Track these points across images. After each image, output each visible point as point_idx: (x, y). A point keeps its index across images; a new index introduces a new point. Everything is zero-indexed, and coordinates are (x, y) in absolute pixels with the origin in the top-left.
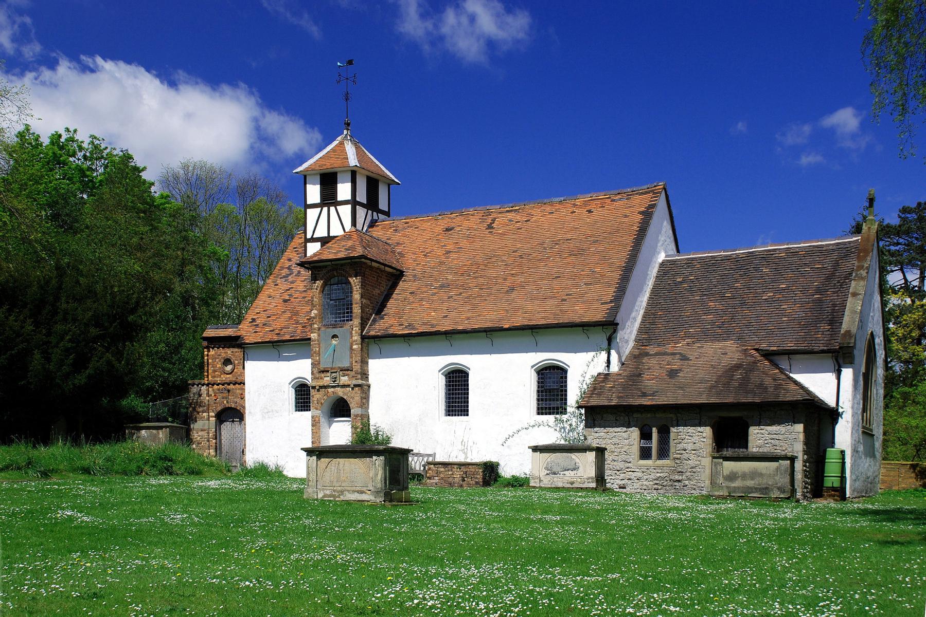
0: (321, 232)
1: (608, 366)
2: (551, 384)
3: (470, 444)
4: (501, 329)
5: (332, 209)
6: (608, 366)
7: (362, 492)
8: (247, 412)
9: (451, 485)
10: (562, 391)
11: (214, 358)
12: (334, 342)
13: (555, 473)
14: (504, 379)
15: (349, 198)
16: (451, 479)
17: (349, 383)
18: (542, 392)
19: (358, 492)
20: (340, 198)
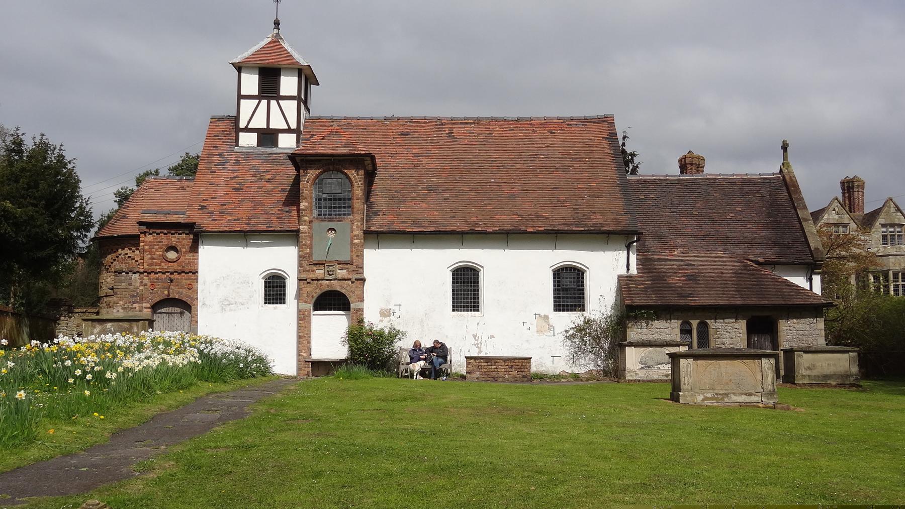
0: (259, 122)
1: (628, 269)
2: (566, 282)
3: (485, 338)
4: (525, 232)
5: (273, 103)
6: (628, 269)
7: (750, 395)
8: (200, 304)
9: (495, 379)
10: (579, 290)
11: (151, 244)
12: (331, 235)
13: (649, 367)
14: (518, 276)
15: (296, 94)
16: (494, 374)
17: (350, 277)
18: (559, 290)
19: (746, 394)
20: (283, 92)
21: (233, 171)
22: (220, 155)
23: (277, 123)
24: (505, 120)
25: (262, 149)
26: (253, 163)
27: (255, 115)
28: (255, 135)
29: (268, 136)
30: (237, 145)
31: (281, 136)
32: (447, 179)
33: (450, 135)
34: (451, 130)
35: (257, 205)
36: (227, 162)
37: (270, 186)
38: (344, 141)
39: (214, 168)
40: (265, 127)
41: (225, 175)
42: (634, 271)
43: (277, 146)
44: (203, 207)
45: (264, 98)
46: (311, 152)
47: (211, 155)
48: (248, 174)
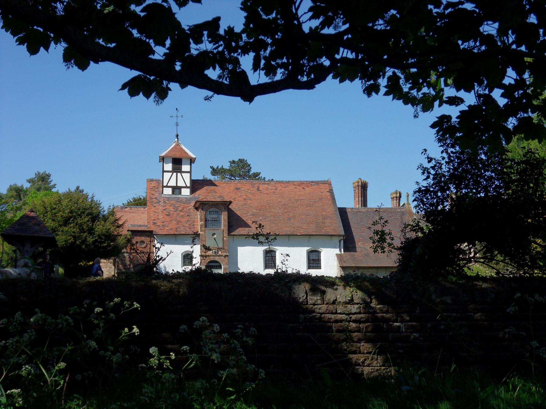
0: (173, 183)
5: (179, 174)
21: (164, 206)
22: (156, 198)
23: (181, 183)
24: (282, 182)
25: (174, 196)
26: (171, 202)
27: (170, 179)
28: (171, 189)
29: (176, 189)
30: (163, 193)
32: (260, 210)
33: (258, 189)
34: (258, 187)
35: (178, 222)
36: (160, 202)
37: (182, 214)
38: (218, 195)
39: (155, 205)
41: (161, 208)
42: (66, 46)
44: (154, 223)
45: (175, 172)
46: (205, 200)
47: (152, 198)
48: (171, 207)
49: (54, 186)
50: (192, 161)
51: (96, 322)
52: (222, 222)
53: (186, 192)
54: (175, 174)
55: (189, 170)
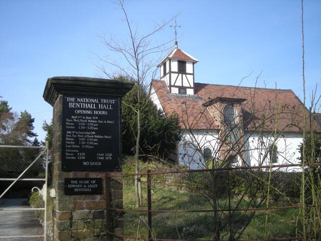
0: (179, 83)
5: (184, 75)
20: (187, 72)
23: (186, 84)
28: (177, 89)
30: (171, 92)
31: (187, 89)
39: (168, 102)
40: (181, 85)
43: (186, 94)
49: (11, 109)
50: (194, 63)
51: (248, 213)
52: (35, 161)
53: (190, 92)
54: (180, 75)
55: (192, 73)
